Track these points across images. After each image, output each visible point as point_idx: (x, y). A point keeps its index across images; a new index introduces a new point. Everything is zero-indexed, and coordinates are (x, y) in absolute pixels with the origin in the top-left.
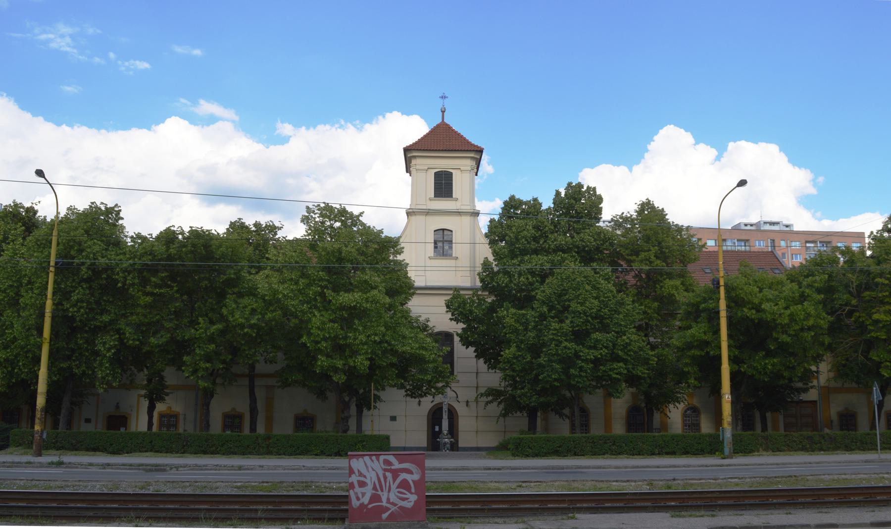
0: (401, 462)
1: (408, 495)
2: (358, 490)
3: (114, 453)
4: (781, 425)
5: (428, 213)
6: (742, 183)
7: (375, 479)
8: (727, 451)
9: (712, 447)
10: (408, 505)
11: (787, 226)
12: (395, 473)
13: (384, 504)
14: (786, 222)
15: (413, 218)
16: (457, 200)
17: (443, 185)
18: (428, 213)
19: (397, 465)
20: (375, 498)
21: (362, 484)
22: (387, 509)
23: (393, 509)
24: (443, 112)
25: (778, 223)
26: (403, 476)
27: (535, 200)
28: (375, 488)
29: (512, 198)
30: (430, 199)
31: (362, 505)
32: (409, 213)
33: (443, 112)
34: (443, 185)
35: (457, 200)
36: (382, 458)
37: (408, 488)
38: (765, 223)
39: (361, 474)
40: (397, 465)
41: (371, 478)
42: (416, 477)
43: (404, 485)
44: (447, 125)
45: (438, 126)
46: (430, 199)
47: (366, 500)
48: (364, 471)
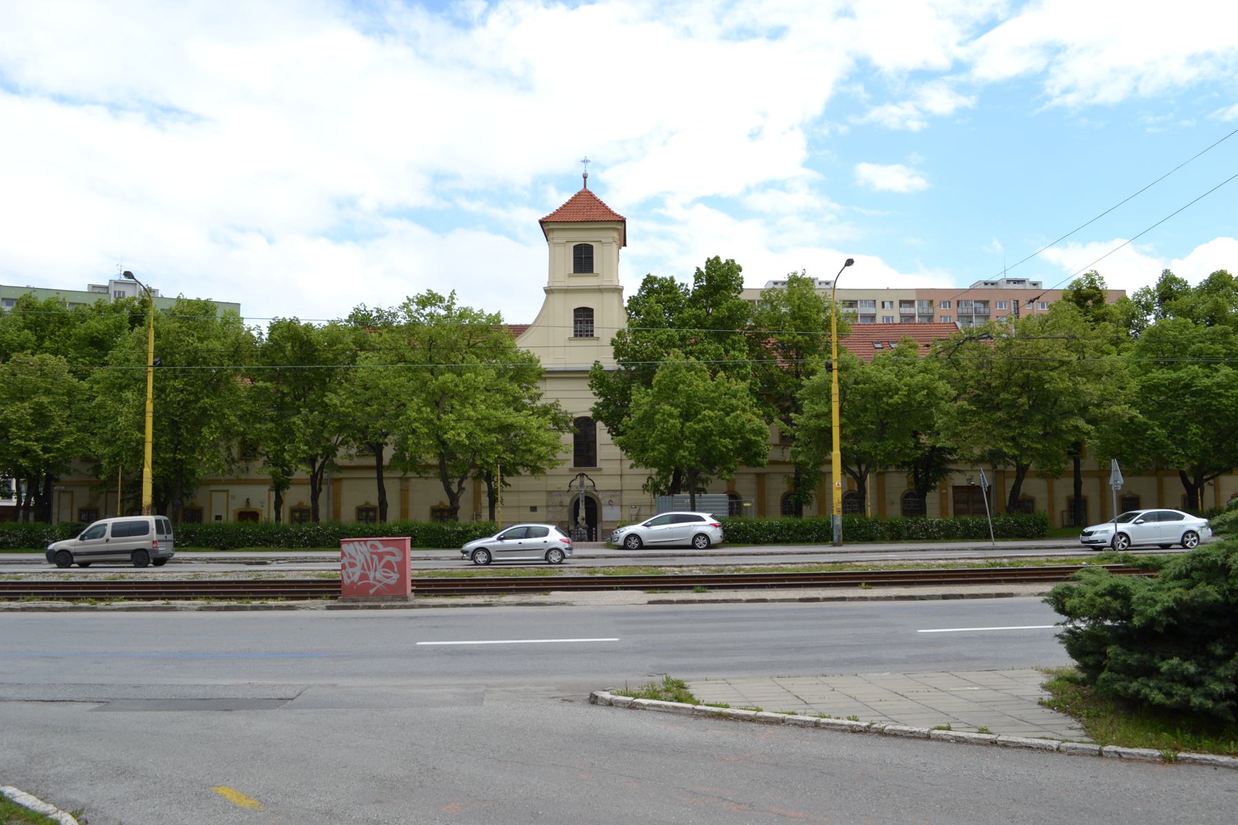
0: (385, 546)
1: (392, 574)
2: (349, 570)
3: (223, 549)
4: (951, 512)
5: (567, 291)
6: (850, 262)
7: (363, 561)
8: (835, 538)
9: (822, 535)
10: (392, 582)
11: (1035, 284)
12: (381, 556)
13: (371, 581)
14: (1033, 279)
15: (551, 296)
16: (597, 275)
17: (583, 260)
18: (567, 291)
19: (382, 549)
20: (364, 577)
21: (352, 565)
22: (374, 586)
23: (379, 585)
24: (585, 178)
25: (1022, 281)
26: (388, 558)
27: (649, 281)
28: (363, 568)
29: (648, 276)
30: (570, 276)
31: (353, 582)
32: (548, 291)
33: (585, 178)
34: (583, 260)
35: (597, 275)
36: (369, 544)
37: (392, 568)
38: (1009, 281)
39: (351, 557)
40: (382, 549)
41: (360, 559)
42: (399, 558)
43: (389, 565)
44: (591, 195)
45: (579, 194)
46: (570, 276)
47: (356, 578)
48: (354, 554)
